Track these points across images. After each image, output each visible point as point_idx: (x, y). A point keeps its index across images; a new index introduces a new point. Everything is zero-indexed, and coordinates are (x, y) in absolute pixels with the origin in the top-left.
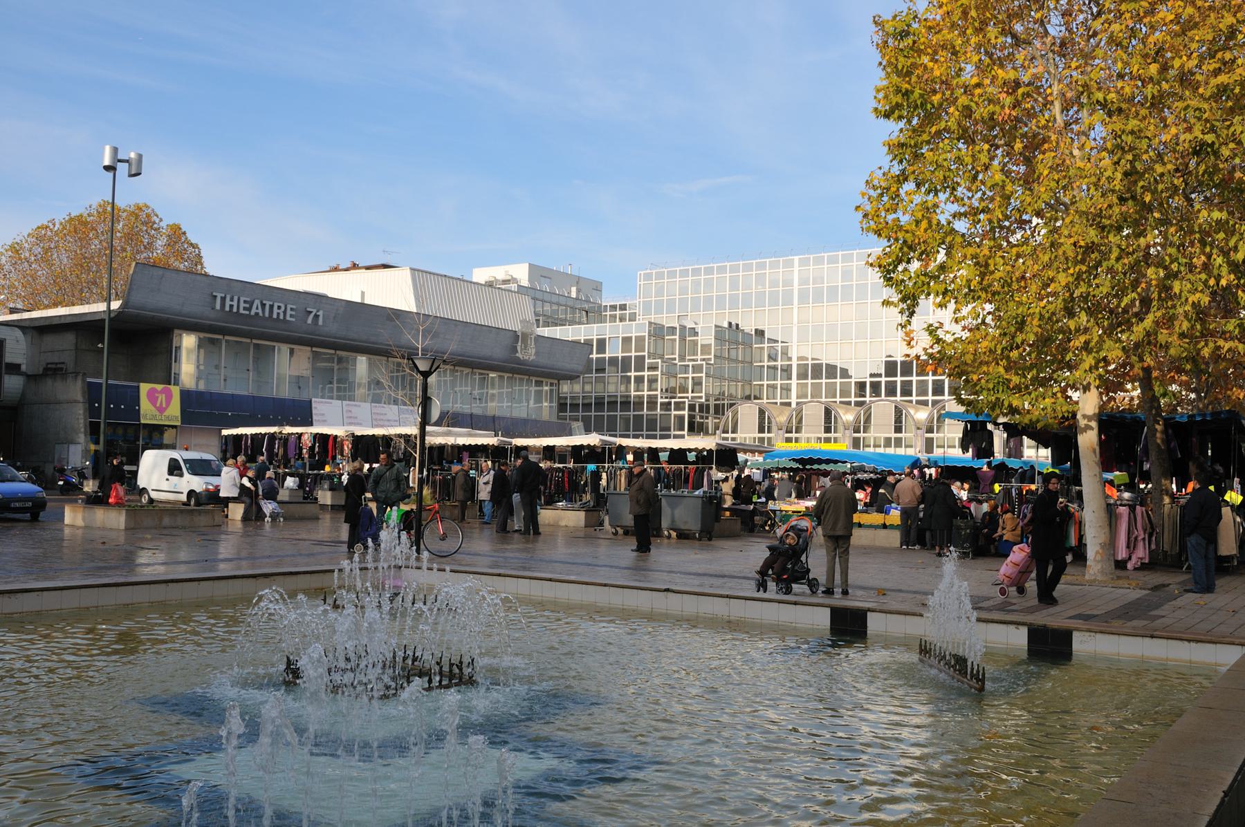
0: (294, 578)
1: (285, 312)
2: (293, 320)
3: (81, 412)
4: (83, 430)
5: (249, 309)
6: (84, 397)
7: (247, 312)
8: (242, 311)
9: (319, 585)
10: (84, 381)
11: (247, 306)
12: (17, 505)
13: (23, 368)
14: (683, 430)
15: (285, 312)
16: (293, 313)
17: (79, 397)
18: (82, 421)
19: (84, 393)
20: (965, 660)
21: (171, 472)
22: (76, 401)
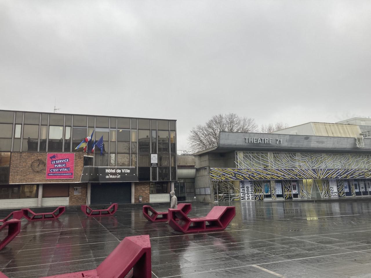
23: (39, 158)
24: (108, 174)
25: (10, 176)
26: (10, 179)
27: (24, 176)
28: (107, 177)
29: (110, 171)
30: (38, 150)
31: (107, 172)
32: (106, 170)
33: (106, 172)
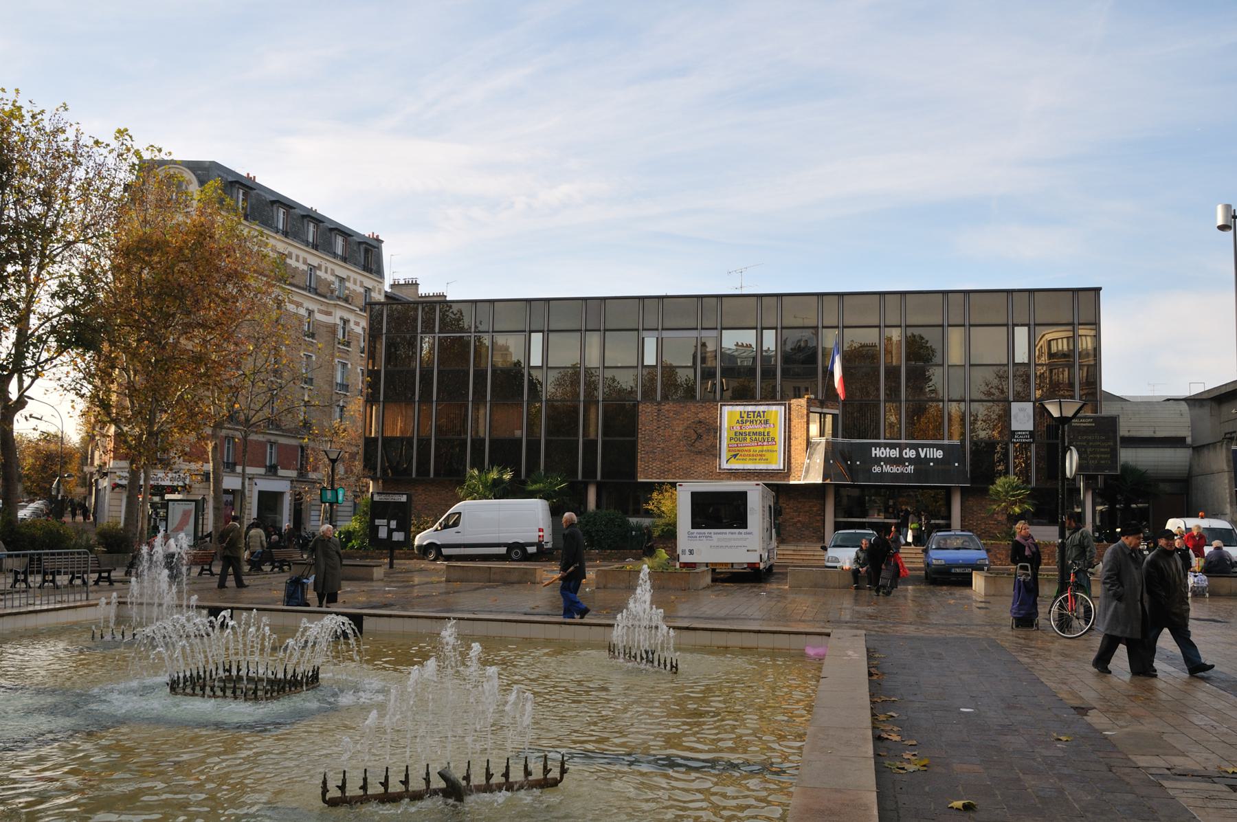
0: (692, 633)
3: (1227, 481)
4: (1228, 500)
6: (1228, 466)
9: (723, 643)
10: (1228, 449)
12: (958, 570)
13: (1189, 440)
17: (1226, 468)
18: (1227, 491)
19: (1228, 461)
20: (171, 689)
22: (1223, 471)
23: (701, 416)
24: (878, 461)
25: (639, 463)
26: (639, 469)
27: (669, 462)
28: (876, 469)
29: (883, 453)
30: (659, 398)
31: (876, 454)
32: (873, 449)
33: (873, 456)
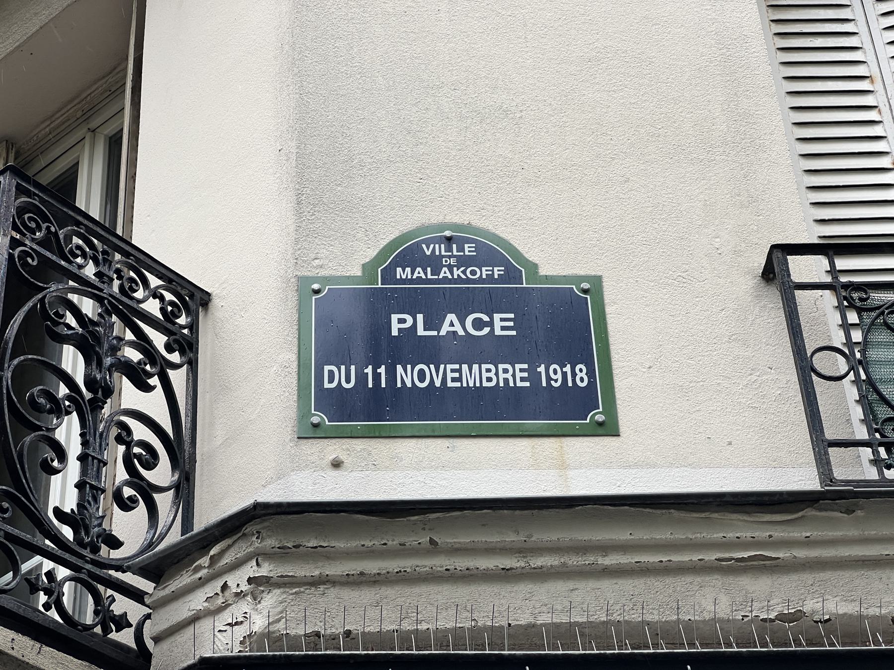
1: (514, 376)
2: (527, 384)
5: (459, 379)
7: (458, 384)
8: (450, 384)
11: (457, 375)
14: (381, 285)
15: (514, 376)
16: (526, 375)
21: (425, 530)
